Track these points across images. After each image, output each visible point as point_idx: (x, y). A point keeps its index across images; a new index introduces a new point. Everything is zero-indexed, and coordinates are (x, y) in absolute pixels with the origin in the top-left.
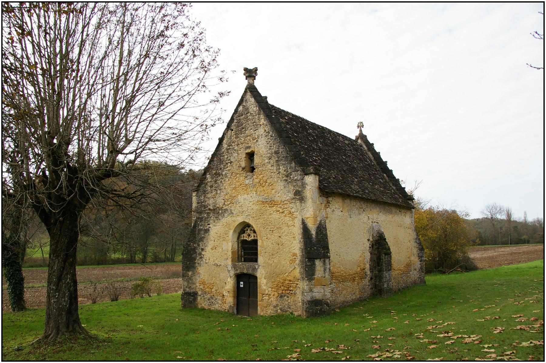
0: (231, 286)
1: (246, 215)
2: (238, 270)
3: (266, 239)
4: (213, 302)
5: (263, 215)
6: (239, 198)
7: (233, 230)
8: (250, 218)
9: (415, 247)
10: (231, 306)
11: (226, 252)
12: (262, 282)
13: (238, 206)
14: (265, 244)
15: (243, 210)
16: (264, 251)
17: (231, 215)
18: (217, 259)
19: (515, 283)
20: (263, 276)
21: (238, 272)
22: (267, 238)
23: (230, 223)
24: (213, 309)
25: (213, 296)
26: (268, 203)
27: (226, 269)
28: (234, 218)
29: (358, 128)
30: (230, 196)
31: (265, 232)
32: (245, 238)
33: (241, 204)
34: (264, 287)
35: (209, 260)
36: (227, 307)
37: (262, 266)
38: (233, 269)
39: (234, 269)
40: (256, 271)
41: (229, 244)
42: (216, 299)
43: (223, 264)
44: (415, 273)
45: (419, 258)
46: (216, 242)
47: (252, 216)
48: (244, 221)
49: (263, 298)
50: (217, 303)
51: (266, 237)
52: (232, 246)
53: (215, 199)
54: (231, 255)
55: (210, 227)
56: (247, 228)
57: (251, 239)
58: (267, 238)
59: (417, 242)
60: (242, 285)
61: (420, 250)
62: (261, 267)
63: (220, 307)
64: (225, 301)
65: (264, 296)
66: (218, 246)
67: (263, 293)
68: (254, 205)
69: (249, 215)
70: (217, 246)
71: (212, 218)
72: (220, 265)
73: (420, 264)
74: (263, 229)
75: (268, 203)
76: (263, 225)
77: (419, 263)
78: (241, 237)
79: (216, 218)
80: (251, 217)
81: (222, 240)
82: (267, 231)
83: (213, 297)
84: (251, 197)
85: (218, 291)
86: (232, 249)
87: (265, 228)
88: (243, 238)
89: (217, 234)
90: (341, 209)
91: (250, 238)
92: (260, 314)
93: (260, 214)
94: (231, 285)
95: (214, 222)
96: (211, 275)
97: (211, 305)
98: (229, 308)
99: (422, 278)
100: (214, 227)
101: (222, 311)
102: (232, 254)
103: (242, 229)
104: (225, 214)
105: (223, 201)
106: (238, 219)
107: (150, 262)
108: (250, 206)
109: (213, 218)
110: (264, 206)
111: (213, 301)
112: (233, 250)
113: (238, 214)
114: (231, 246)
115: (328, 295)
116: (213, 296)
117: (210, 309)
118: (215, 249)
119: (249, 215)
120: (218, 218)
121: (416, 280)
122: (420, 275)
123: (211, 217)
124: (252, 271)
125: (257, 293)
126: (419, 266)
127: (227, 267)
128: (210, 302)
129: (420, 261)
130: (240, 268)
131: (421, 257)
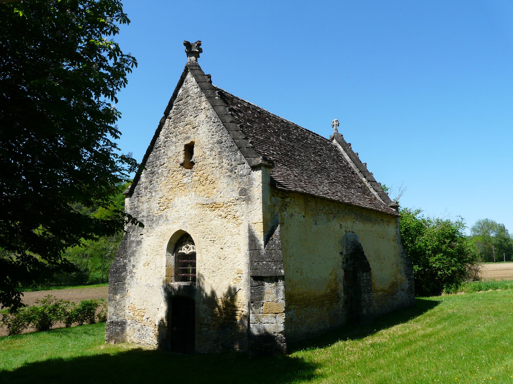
9: (401, 263)
52: (167, 261)
59: (403, 257)
61: (407, 266)
73: (409, 283)
77: (407, 282)
90: (303, 213)
99: (412, 300)
122: (408, 297)
126: (408, 285)
129: (409, 280)
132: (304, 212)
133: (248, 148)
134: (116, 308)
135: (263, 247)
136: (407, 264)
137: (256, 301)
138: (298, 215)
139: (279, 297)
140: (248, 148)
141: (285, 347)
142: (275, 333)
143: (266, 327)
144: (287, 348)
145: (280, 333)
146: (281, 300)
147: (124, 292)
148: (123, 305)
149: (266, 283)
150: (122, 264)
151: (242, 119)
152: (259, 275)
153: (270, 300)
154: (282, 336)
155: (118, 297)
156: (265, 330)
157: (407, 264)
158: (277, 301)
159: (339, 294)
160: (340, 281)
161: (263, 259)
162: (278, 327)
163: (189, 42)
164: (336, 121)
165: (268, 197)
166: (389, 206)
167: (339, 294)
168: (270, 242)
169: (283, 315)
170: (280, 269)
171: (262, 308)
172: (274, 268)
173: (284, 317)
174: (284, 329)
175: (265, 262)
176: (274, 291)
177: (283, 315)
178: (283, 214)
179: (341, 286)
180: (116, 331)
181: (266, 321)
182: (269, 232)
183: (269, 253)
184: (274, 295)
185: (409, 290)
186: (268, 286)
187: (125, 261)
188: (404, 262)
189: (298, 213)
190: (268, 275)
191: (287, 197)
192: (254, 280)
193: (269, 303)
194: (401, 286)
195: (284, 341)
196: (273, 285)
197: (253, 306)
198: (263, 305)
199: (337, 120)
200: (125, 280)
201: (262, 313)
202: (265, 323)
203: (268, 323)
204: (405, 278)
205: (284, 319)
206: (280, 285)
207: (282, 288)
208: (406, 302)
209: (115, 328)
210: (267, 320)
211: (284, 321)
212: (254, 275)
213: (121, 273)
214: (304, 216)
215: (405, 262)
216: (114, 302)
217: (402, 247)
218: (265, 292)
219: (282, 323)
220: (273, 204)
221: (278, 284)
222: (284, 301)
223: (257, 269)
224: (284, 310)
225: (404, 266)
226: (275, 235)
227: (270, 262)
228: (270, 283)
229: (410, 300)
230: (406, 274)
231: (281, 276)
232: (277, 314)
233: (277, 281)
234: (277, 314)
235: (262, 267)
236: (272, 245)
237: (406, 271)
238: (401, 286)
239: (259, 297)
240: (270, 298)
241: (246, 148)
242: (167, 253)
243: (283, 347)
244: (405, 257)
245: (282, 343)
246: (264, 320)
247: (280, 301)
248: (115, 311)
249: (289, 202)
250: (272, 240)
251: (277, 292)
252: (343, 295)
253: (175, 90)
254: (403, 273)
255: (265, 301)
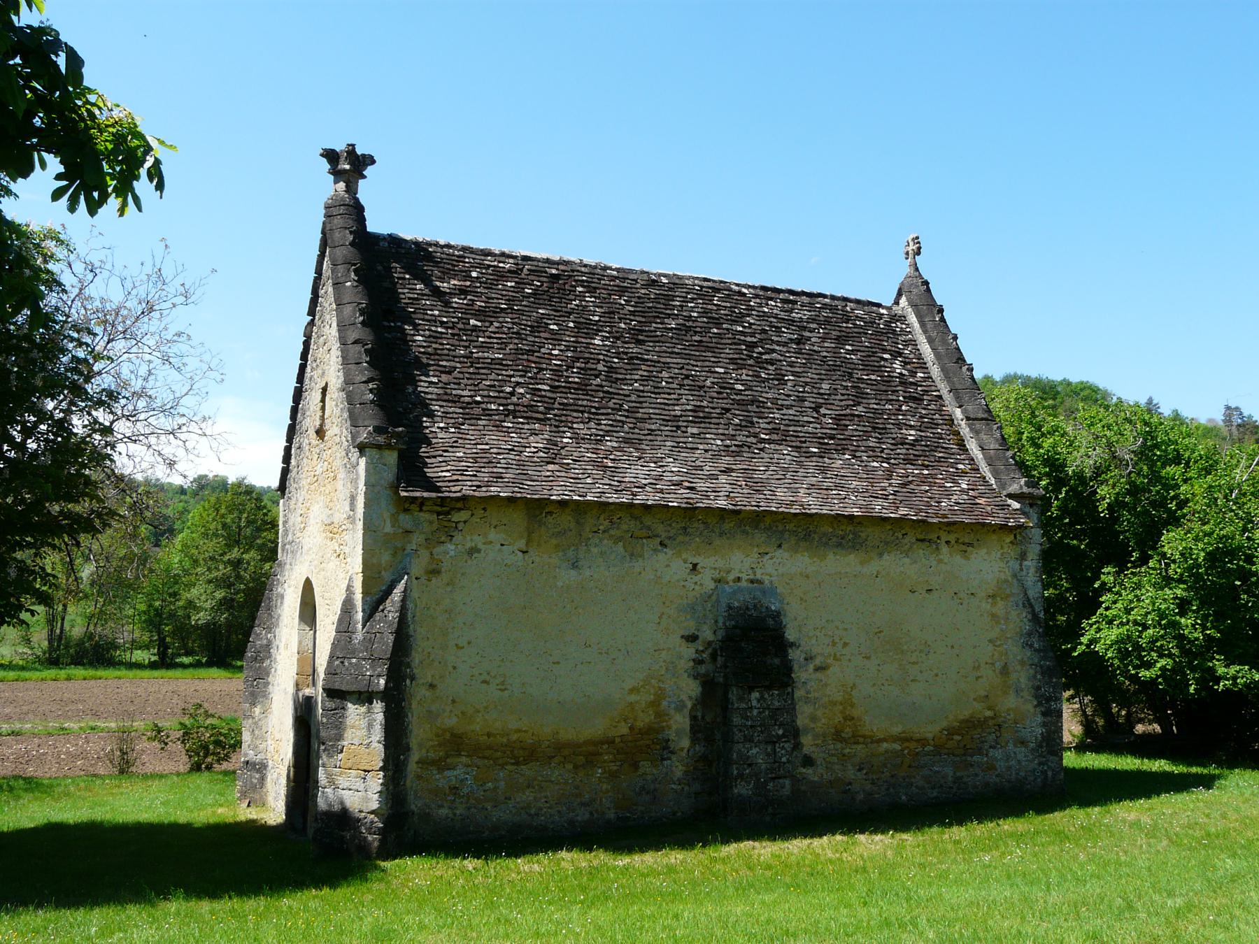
9: (1022, 663)
19: (324, 390)
29: (907, 258)
44: (1020, 757)
45: (1040, 704)
52: (300, 643)
59: (1031, 646)
61: (1043, 674)
73: (1044, 724)
77: (1039, 719)
90: (522, 544)
99: (1050, 773)
107: (315, 690)
115: (478, 729)
121: (1025, 778)
122: (1040, 764)
125: (805, 835)
126: (1039, 730)
129: (1044, 714)
131: (1048, 700)
132: (523, 541)
133: (364, 404)
134: (254, 735)
135: (360, 626)
136: (1041, 667)
137: (330, 741)
138: (500, 550)
139: (373, 736)
140: (364, 404)
141: (376, 844)
142: (361, 811)
143: (345, 797)
144: (379, 847)
145: (372, 812)
146: (377, 745)
147: (267, 701)
148: (264, 730)
149: (350, 705)
150: (265, 642)
151: (454, 312)
152: (337, 688)
153: (356, 742)
154: (376, 819)
155: (257, 710)
156: (342, 803)
157: (1041, 667)
158: (368, 745)
159: (669, 740)
160: (680, 707)
161: (353, 653)
162: (367, 800)
163: (334, 150)
164: (913, 240)
165: (387, 515)
166: (1005, 493)
167: (669, 740)
168: (378, 616)
169: (379, 776)
170: (379, 676)
171: (340, 756)
172: (368, 673)
173: (381, 781)
174: (378, 806)
175: (354, 660)
176: (364, 723)
177: (379, 776)
178: (438, 550)
179: (680, 722)
180: (252, 782)
181: (346, 785)
182: (381, 593)
183: (369, 641)
184: (364, 732)
185: (1044, 745)
186: (354, 712)
187: (269, 635)
188: (1031, 662)
189: (502, 545)
190: (353, 688)
191: (460, 509)
192: (328, 696)
193: (353, 747)
194: (1017, 732)
195: (375, 832)
196: (363, 709)
197: (324, 750)
198: (342, 751)
199: (915, 236)
200: (268, 676)
201: (340, 767)
202: (343, 789)
203: (350, 790)
204: (1032, 710)
205: (381, 785)
206: (376, 711)
207: (380, 717)
208: (1032, 778)
209: (251, 775)
210: (348, 784)
211: (379, 789)
212: (326, 687)
213: (262, 661)
214: (525, 549)
215: (1036, 661)
216: (250, 721)
217: (1030, 617)
218: (348, 723)
219: (375, 792)
220: (401, 530)
221: (372, 708)
222: (381, 746)
223: (336, 674)
224: (381, 764)
225: (1032, 672)
226: (392, 601)
227: (364, 659)
228: (356, 706)
229: (1044, 773)
230: (1036, 697)
231: (377, 692)
232: (369, 771)
233: (371, 703)
234: (369, 771)
235: (347, 669)
236: (380, 621)
237: (1038, 688)
238: (1017, 732)
239: (336, 734)
240: (356, 736)
241: (360, 404)
242: (299, 624)
243: (370, 844)
244: (1036, 646)
245: (370, 834)
246: (342, 782)
247: (375, 745)
248: (252, 741)
249: (465, 522)
250: (383, 611)
251: (370, 726)
252: (686, 743)
253: (317, 262)
254: (1025, 694)
255: (345, 743)
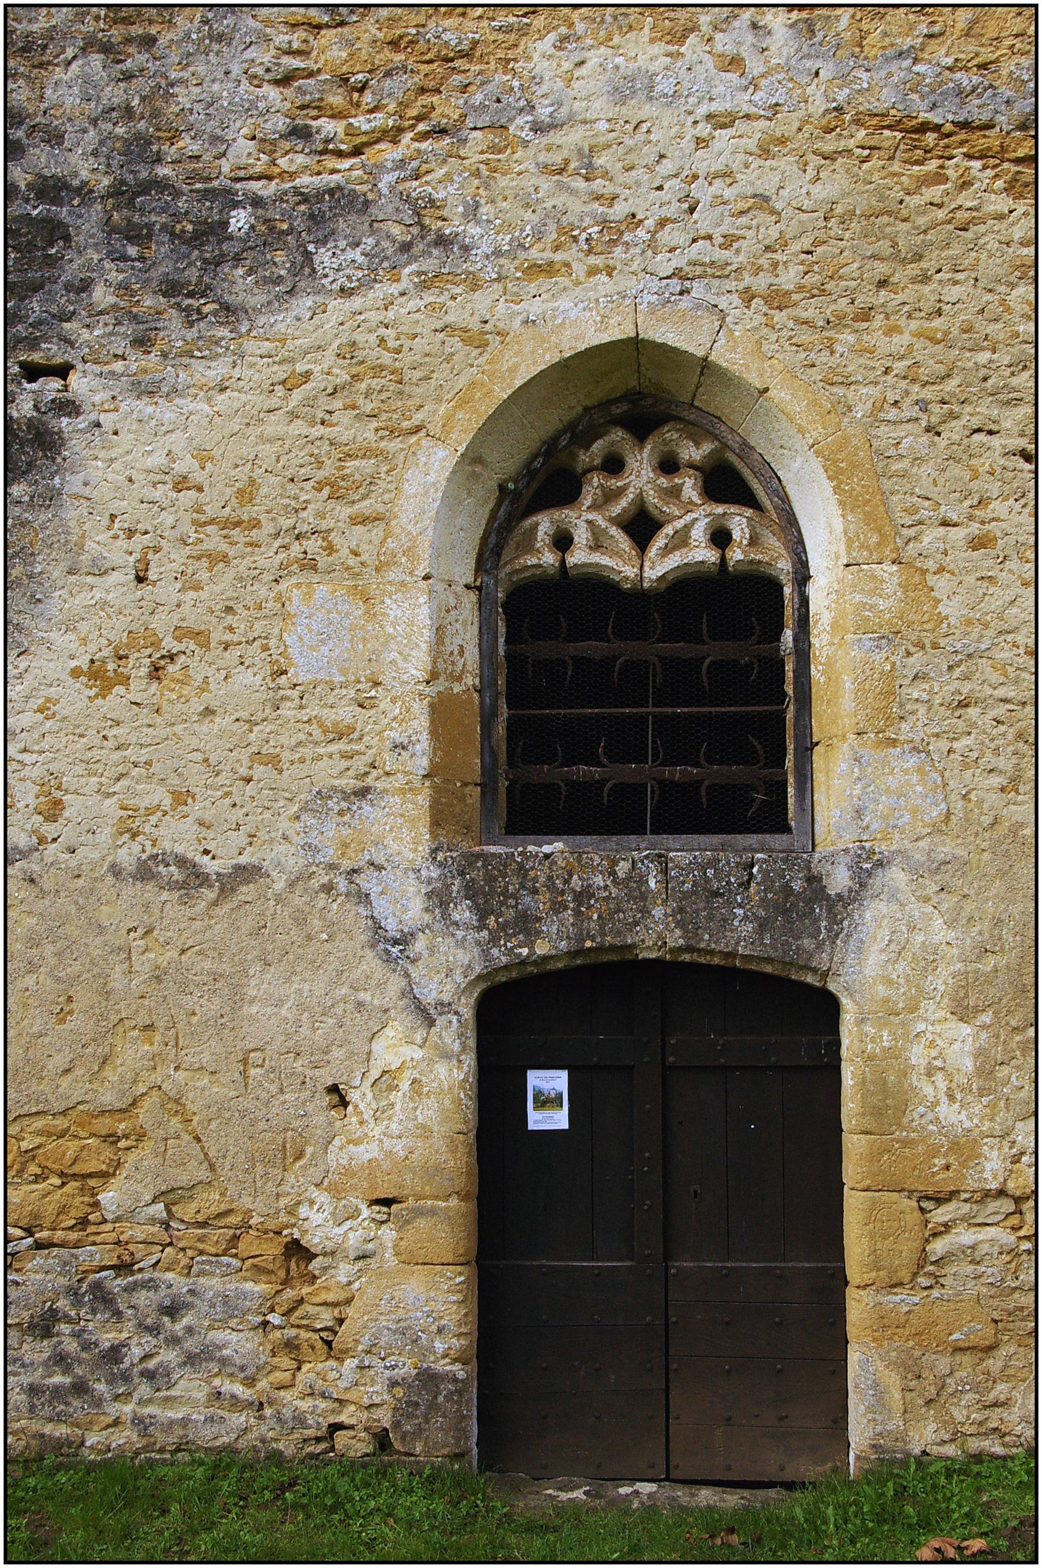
0: (425, 1131)
1: (664, 264)
2: (550, 927)
3: (960, 557)
4: (115, 1354)
5: (925, 279)
6: (540, 66)
7: (462, 440)
8: (730, 302)
10: (428, 1379)
11: (345, 713)
12: (918, 1055)
13: (524, 160)
14: (952, 609)
15: (620, 210)
16: (947, 688)
17: (430, 265)
18: (181, 798)
20: (941, 981)
21: (542, 948)
22: (978, 543)
23: (407, 359)
24: (124, 1438)
25: (123, 1268)
26: (992, 140)
27: (354, 916)
28: (481, 301)
30: (394, 44)
31: (956, 470)
32: (579, 556)
33: (572, 138)
34: (950, 1114)
35: (53, 810)
36: (376, 1390)
37: (916, 872)
38: (463, 913)
39: (483, 914)
40: (834, 919)
41: (394, 608)
42: (172, 1311)
43: (295, 862)
46: (167, 591)
47: (761, 283)
48: (635, 345)
49: (938, 1247)
50: (191, 1360)
51: (957, 535)
52: (440, 631)
53: (136, 59)
54: (423, 743)
55: (69, 407)
56: (618, 434)
57: (674, 561)
58: (978, 543)
60: (545, 1102)
62: (897, 876)
63: (236, 1404)
64: (326, 1317)
65: (941, 1214)
66: (200, 637)
67: (944, 1181)
68: (786, 163)
69: (717, 271)
70: (181, 633)
71: (102, 296)
72: (246, 873)
74: (912, 439)
75: (992, 140)
76: (928, 393)
78: (528, 544)
79: (171, 288)
80: (748, 296)
81: (269, 559)
82: (983, 464)
83: (116, 1284)
84: (734, 63)
85: (210, 1202)
86: (433, 677)
87: (954, 431)
88: (549, 558)
89: (181, 484)
91: (667, 551)
92: (901, 1437)
93: (881, 269)
94: (428, 1112)
95: (142, 343)
96: (84, 998)
97: (80, 1388)
98: (404, 1410)
100: (144, 407)
101: (276, 1458)
102: (434, 733)
103: (550, 448)
104: (323, 258)
105: (272, 93)
106: (534, 308)
108: (727, 174)
109: (124, 288)
110: (938, 178)
111: (108, 1338)
112: (441, 685)
113: (535, 254)
114: (425, 636)
116: (123, 1268)
117: (59, 1445)
118: (156, 672)
119: (717, 271)
120: (204, 291)
123: (85, 286)
124: (763, 926)
127: (364, 898)
128: (61, 1360)
130: (583, 896)
